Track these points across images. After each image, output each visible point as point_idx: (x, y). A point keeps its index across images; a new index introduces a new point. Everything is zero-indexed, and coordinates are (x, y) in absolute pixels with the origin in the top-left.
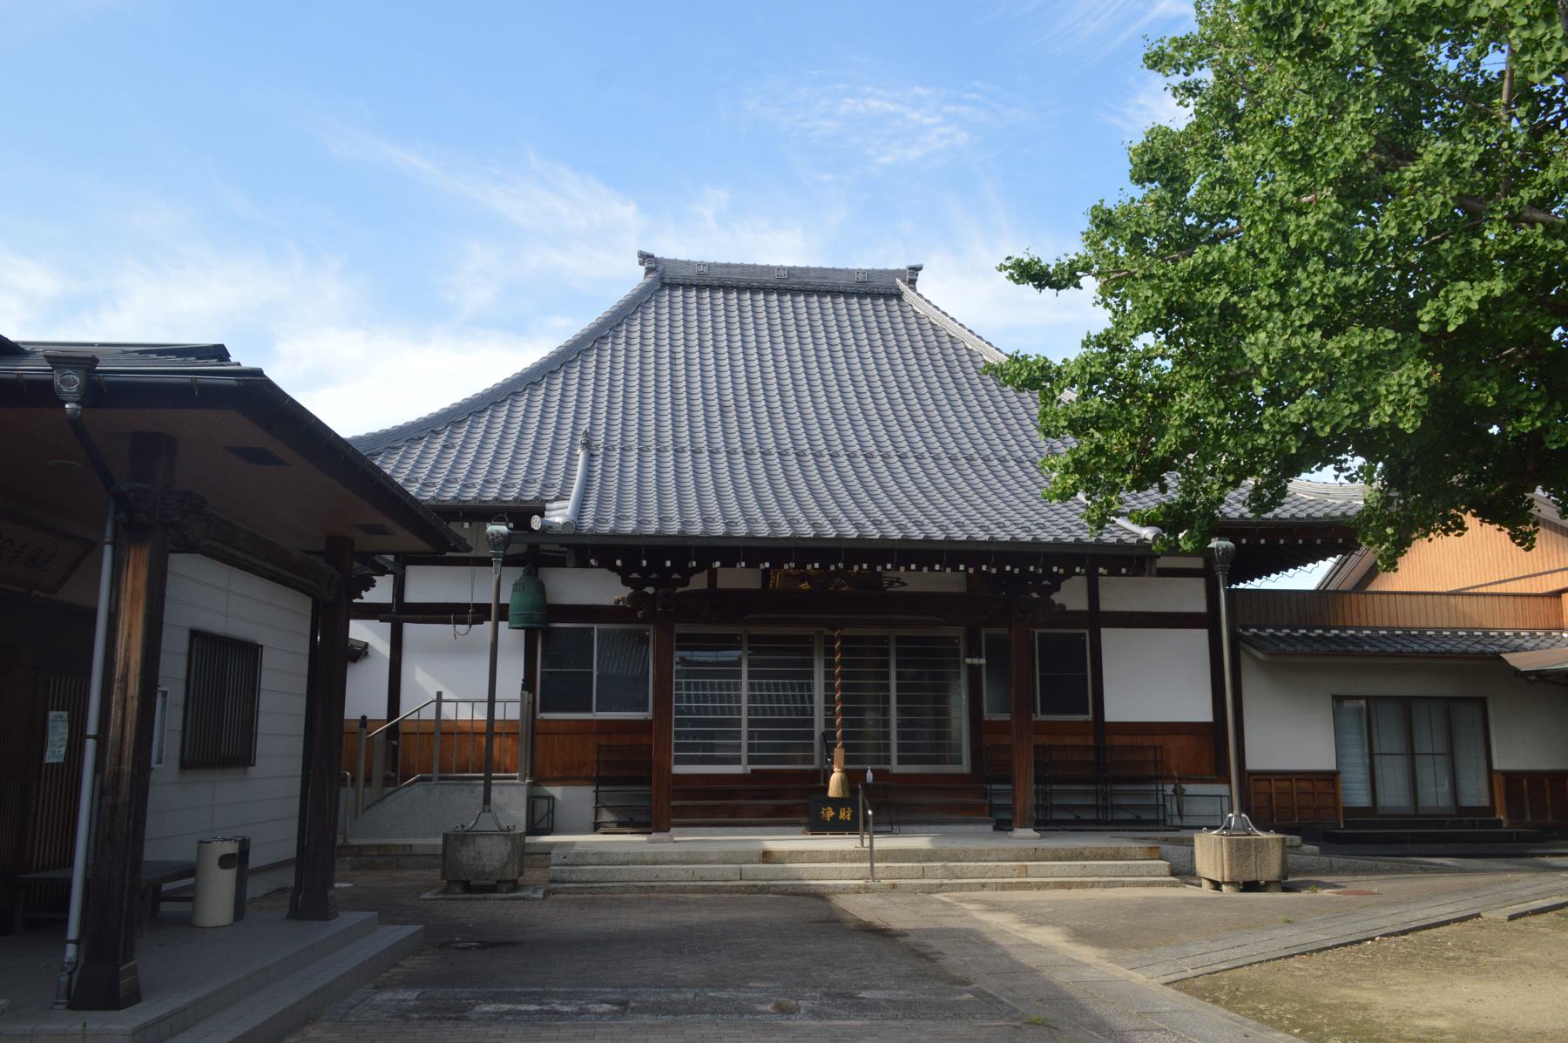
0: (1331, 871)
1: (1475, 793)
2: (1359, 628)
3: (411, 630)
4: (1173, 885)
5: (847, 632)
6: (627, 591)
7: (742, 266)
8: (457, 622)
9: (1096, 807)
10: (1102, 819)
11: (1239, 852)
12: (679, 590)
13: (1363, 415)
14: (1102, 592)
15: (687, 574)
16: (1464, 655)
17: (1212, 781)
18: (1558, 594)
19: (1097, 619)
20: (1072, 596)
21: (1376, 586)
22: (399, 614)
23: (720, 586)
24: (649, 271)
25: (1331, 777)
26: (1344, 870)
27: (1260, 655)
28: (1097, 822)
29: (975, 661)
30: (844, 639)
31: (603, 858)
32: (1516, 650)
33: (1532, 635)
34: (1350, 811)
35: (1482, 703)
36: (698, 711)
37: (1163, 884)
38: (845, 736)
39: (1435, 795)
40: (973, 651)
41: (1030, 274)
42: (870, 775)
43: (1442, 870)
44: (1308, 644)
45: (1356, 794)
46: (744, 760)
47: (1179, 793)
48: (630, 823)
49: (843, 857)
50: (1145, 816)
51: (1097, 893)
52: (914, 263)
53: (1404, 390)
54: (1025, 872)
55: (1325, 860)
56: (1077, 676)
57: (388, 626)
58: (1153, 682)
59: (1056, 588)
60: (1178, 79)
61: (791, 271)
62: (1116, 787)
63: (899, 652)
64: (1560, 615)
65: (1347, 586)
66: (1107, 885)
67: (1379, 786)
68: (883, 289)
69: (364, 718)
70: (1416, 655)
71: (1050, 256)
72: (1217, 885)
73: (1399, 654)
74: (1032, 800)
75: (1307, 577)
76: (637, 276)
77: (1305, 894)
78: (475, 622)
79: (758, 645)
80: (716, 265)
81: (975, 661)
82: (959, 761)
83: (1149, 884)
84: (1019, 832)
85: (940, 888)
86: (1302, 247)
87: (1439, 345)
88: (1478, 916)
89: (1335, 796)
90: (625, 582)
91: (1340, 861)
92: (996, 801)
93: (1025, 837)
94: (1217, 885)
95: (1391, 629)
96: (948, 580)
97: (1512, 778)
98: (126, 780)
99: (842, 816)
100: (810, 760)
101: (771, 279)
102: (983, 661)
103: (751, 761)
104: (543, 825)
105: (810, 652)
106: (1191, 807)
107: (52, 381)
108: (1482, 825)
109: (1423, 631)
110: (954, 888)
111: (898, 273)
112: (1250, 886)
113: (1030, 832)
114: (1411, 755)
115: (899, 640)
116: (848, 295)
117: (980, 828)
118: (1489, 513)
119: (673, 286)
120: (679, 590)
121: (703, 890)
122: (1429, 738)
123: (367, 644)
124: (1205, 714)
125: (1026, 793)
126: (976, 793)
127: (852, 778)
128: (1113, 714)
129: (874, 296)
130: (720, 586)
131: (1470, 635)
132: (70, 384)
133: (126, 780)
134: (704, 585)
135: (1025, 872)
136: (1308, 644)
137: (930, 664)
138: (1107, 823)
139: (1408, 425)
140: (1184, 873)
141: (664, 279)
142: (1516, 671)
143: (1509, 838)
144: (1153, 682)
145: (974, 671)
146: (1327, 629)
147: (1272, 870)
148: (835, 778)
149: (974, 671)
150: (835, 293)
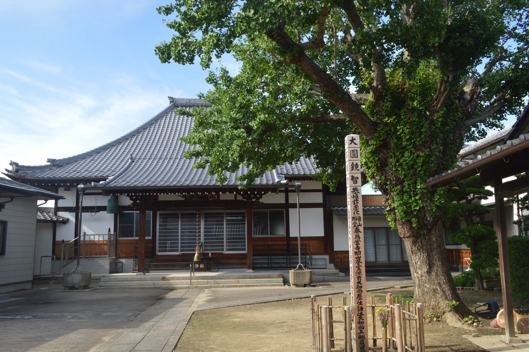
2: (370, 207)
6: (132, 202)
8: (91, 212)
9: (268, 263)
14: (289, 198)
24: (171, 102)
36: (218, 235)
42: (210, 254)
43: (380, 280)
46: (179, 250)
47: (311, 258)
51: (238, 289)
54: (239, 282)
57: (75, 213)
59: (261, 197)
62: (292, 257)
67: (378, 255)
69: (63, 240)
76: (167, 104)
78: (96, 212)
88: (343, 293)
90: (131, 199)
99: (201, 267)
103: (182, 250)
104: (120, 270)
110: (217, 287)
113: (251, 271)
114: (388, 245)
123: (68, 219)
124: (320, 233)
135: (239, 282)
140: (286, 282)
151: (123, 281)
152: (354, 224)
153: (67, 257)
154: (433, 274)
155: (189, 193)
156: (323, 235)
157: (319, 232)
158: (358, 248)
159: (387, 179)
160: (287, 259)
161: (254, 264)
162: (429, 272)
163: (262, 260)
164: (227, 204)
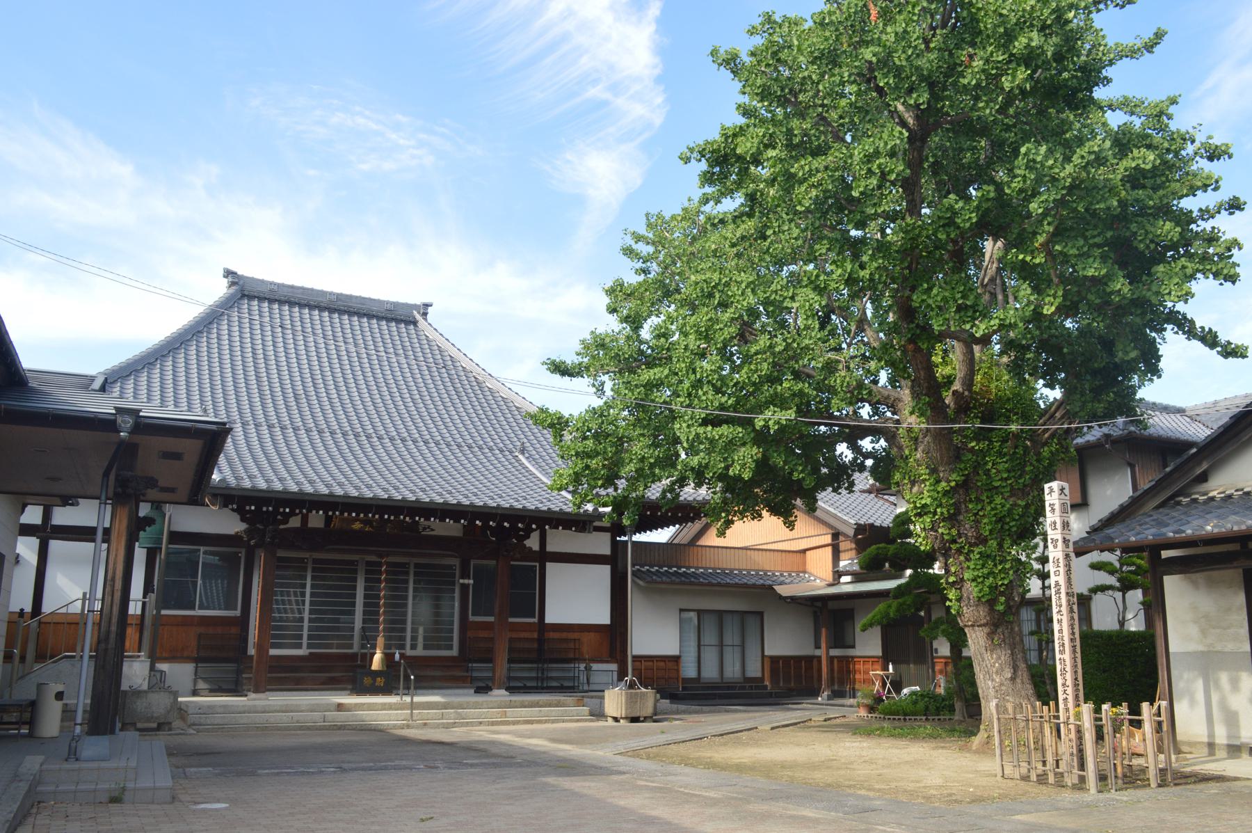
0: (678, 712)
1: (754, 670)
2: (697, 568)
3: (55, 545)
4: (592, 721)
5: (391, 559)
7: (303, 288)
9: (537, 679)
10: (541, 685)
11: (631, 701)
12: (282, 527)
13: (727, 468)
15: (287, 517)
16: (754, 586)
17: (607, 662)
18: (804, 551)
19: (545, 557)
20: (533, 543)
21: (701, 542)
22: (46, 533)
23: (310, 525)
24: (232, 284)
25: (676, 659)
26: (684, 712)
27: (641, 583)
28: (536, 688)
29: (466, 581)
30: (388, 564)
31: (211, 709)
32: (781, 583)
33: (790, 575)
34: (686, 680)
35: (761, 614)
37: (586, 720)
38: (385, 630)
39: (733, 671)
40: (465, 575)
41: (560, 369)
43: (736, 711)
44: (671, 575)
45: (689, 671)
46: (305, 645)
47: (588, 669)
48: (217, 690)
49: (391, 707)
50: (566, 684)
52: (427, 301)
53: (744, 460)
55: (674, 706)
56: (529, 594)
58: (577, 598)
60: (640, 265)
61: (340, 297)
63: (416, 574)
64: (804, 563)
65: (685, 541)
66: (553, 722)
68: (402, 317)
69: (22, 610)
70: (728, 585)
71: (571, 359)
72: (616, 719)
73: (719, 584)
74: (505, 671)
75: (661, 536)
76: (219, 289)
77: (665, 723)
79: (321, 568)
80: (284, 285)
81: (466, 581)
82: (450, 647)
83: (578, 721)
84: (496, 692)
85: (454, 725)
86: (700, 381)
87: (761, 437)
89: (678, 671)
91: (682, 707)
92: (475, 674)
93: (499, 694)
94: (616, 719)
95: (714, 569)
96: (449, 528)
97: (774, 660)
98: (113, 636)
100: (351, 646)
101: (324, 301)
102: (471, 582)
105: (355, 571)
106: (595, 678)
107: (115, 421)
108: (757, 688)
109: (732, 570)
110: (462, 725)
111: (415, 307)
112: (634, 720)
113: (503, 692)
114: (721, 646)
115: (417, 565)
116: (379, 318)
117: (466, 691)
118: (774, 511)
119: (251, 298)
120: (282, 527)
121: (301, 728)
122: (731, 637)
125: (502, 666)
126: (464, 668)
127: (388, 658)
128: (550, 618)
129: (398, 321)
130: (310, 525)
131: (757, 574)
132: (127, 423)
133: (113, 636)
134: (298, 525)
136: (671, 575)
137: (445, 584)
138: (543, 688)
139: (746, 476)
140: (599, 714)
141: (244, 291)
142: (780, 596)
143: (770, 695)
144: (577, 598)
145: (464, 588)
146: (679, 568)
147: (648, 711)
148: (378, 657)
149: (464, 588)
150: (370, 316)
151: (536, 688)
152: (1068, 601)
153: (30, 655)
154: (1019, 681)
155: (397, 516)
156: (607, 621)
157: (601, 615)
158: (1073, 634)
159: (960, 535)
160: (538, 669)
161: (510, 678)
162: (1013, 679)
163: (526, 671)
164: (305, 536)
